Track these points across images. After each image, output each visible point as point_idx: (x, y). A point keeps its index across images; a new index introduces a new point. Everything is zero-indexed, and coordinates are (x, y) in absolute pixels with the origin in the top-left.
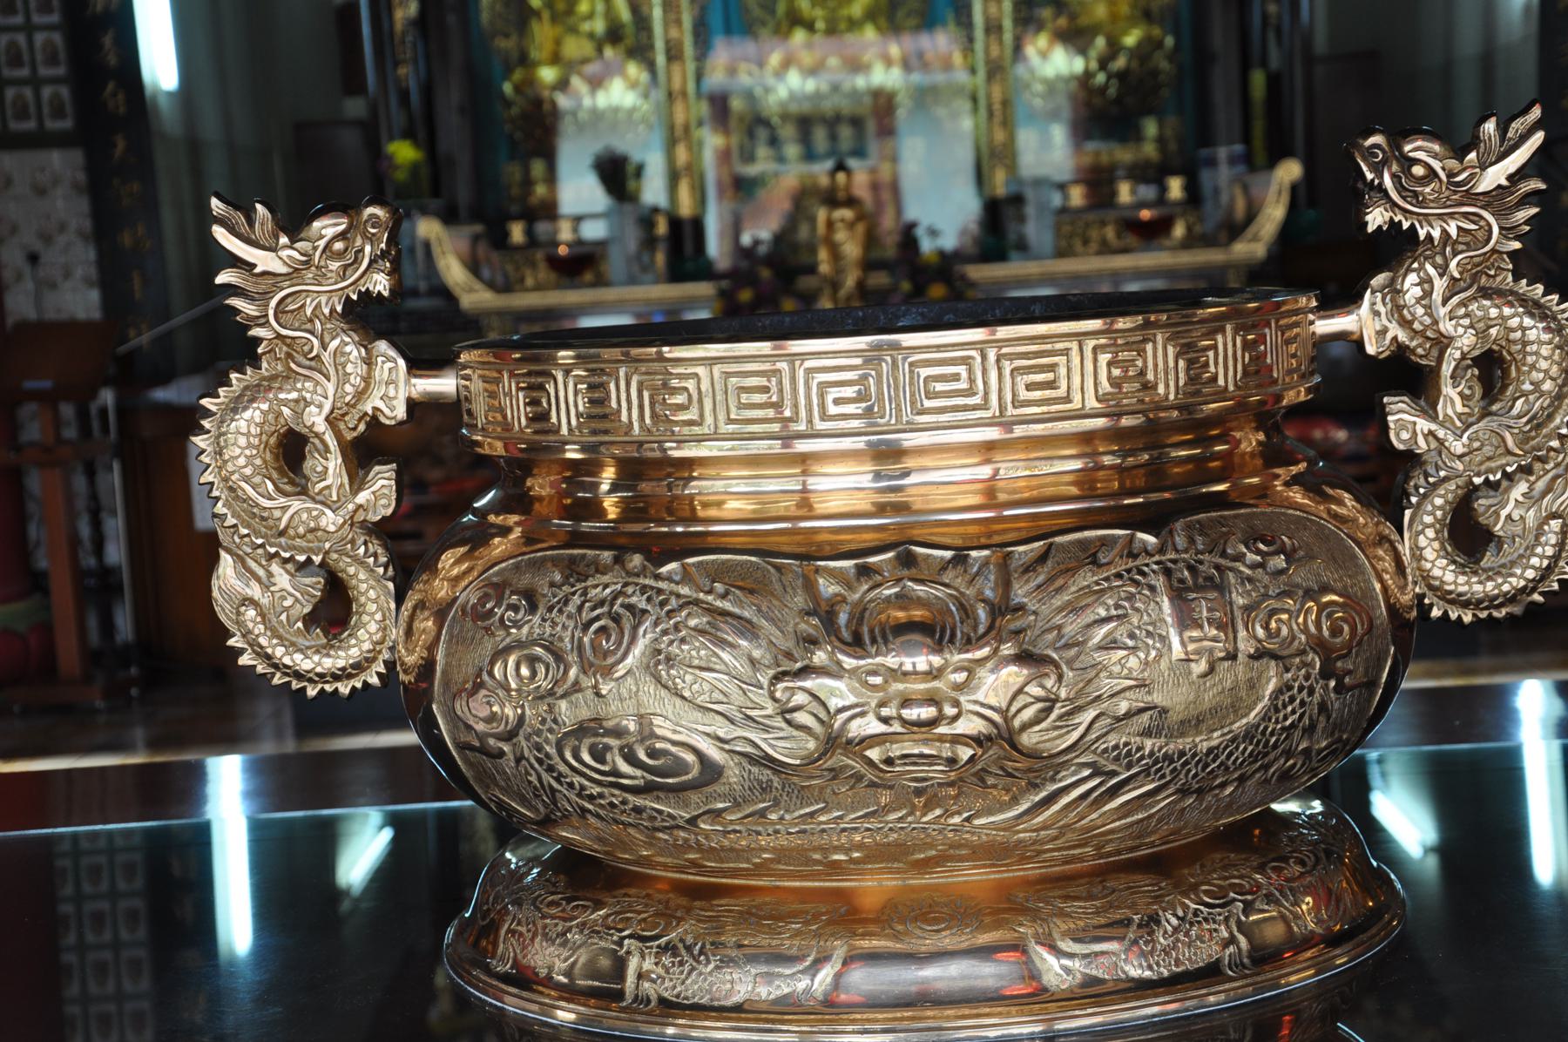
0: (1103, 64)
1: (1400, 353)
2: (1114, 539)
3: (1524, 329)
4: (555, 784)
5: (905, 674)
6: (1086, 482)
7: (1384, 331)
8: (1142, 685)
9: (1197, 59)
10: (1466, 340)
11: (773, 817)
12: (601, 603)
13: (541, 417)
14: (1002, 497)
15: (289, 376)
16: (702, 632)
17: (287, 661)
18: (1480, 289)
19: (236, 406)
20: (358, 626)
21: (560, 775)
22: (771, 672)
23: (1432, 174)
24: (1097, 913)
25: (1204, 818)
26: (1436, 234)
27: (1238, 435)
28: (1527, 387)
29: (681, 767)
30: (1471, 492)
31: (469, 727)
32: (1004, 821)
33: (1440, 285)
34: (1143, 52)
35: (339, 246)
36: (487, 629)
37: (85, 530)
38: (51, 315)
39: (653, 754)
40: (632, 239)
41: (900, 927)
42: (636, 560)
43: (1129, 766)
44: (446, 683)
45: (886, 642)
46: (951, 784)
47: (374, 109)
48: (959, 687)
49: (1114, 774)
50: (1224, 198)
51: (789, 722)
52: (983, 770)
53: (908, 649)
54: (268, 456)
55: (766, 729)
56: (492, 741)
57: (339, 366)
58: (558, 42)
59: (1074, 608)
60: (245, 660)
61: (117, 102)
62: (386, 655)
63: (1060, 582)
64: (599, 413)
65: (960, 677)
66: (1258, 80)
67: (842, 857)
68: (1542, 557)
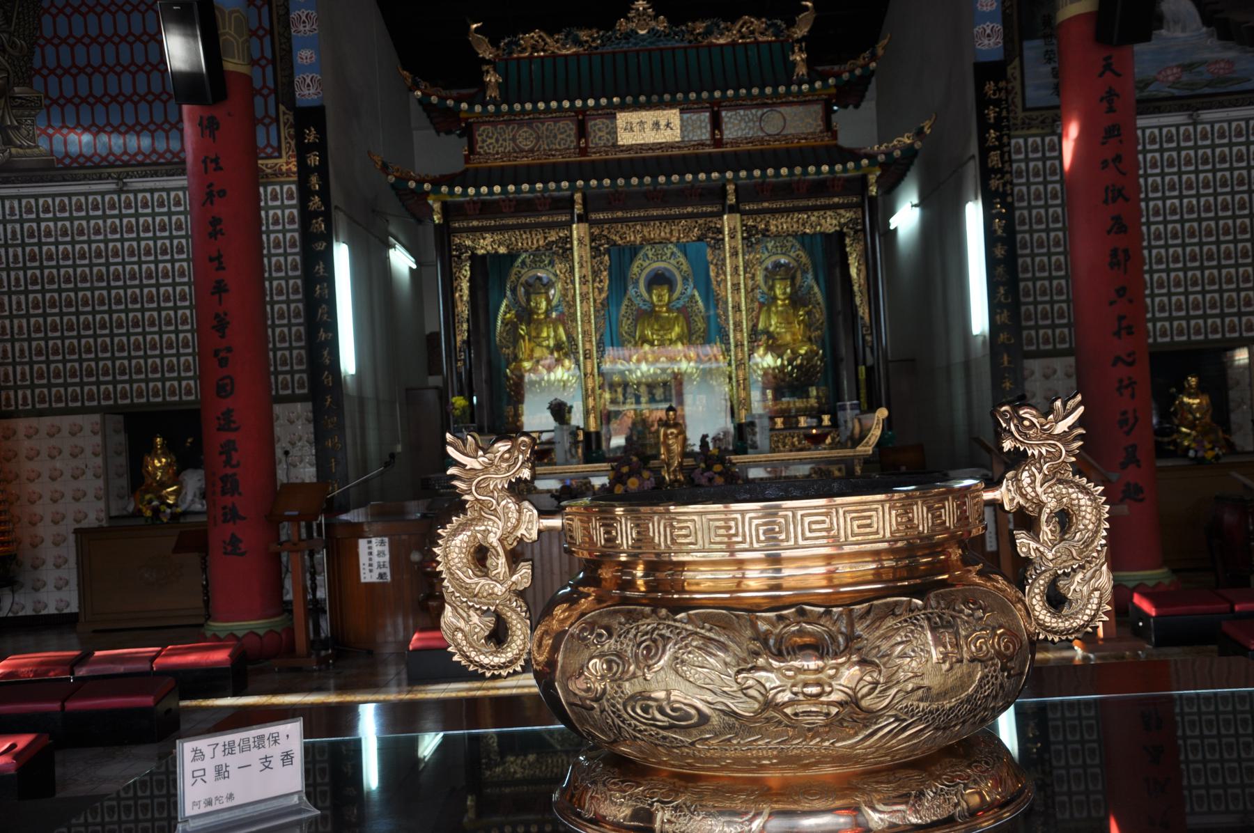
0: (790, 362)
1: (1021, 510)
2: (902, 602)
3: (1079, 499)
4: (621, 724)
5: (805, 670)
6: (877, 576)
7: (1013, 499)
8: (916, 676)
9: (834, 361)
10: (1051, 504)
11: (735, 742)
12: (647, 633)
13: (610, 540)
14: (836, 582)
15: (481, 519)
16: (700, 648)
17: (477, 659)
18: (1058, 480)
19: (455, 533)
20: (511, 642)
21: (624, 719)
22: (736, 669)
23: (1033, 425)
24: (894, 790)
25: (943, 739)
26: (1036, 453)
27: (950, 550)
28: (1081, 527)
29: (688, 716)
30: (1056, 577)
31: (575, 695)
32: (849, 745)
33: (1039, 477)
34: (809, 356)
35: (507, 456)
36: (586, 645)
37: (309, 583)
38: (293, 480)
39: (673, 710)
40: (567, 442)
41: (796, 798)
42: (664, 612)
43: (912, 717)
44: (563, 672)
45: (795, 654)
46: (825, 726)
47: (445, 382)
48: (831, 677)
49: (905, 720)
50: (850, 425)
51: (745, 694)
52: (842, 719)
53: (806, 658)
54: (470, 558)
55: (733, 697)
56: (588, 702)
57: (506, 514)
58: (532, 350)
59: (885, 637)
60: (456, 658)
61: (327, 379)
62: (525, 656)
63: (878, 624)
64: (642, 539)
65: (832, 672)
66: (862, 369)
67: (767, 762)
68: (1091, 610)
